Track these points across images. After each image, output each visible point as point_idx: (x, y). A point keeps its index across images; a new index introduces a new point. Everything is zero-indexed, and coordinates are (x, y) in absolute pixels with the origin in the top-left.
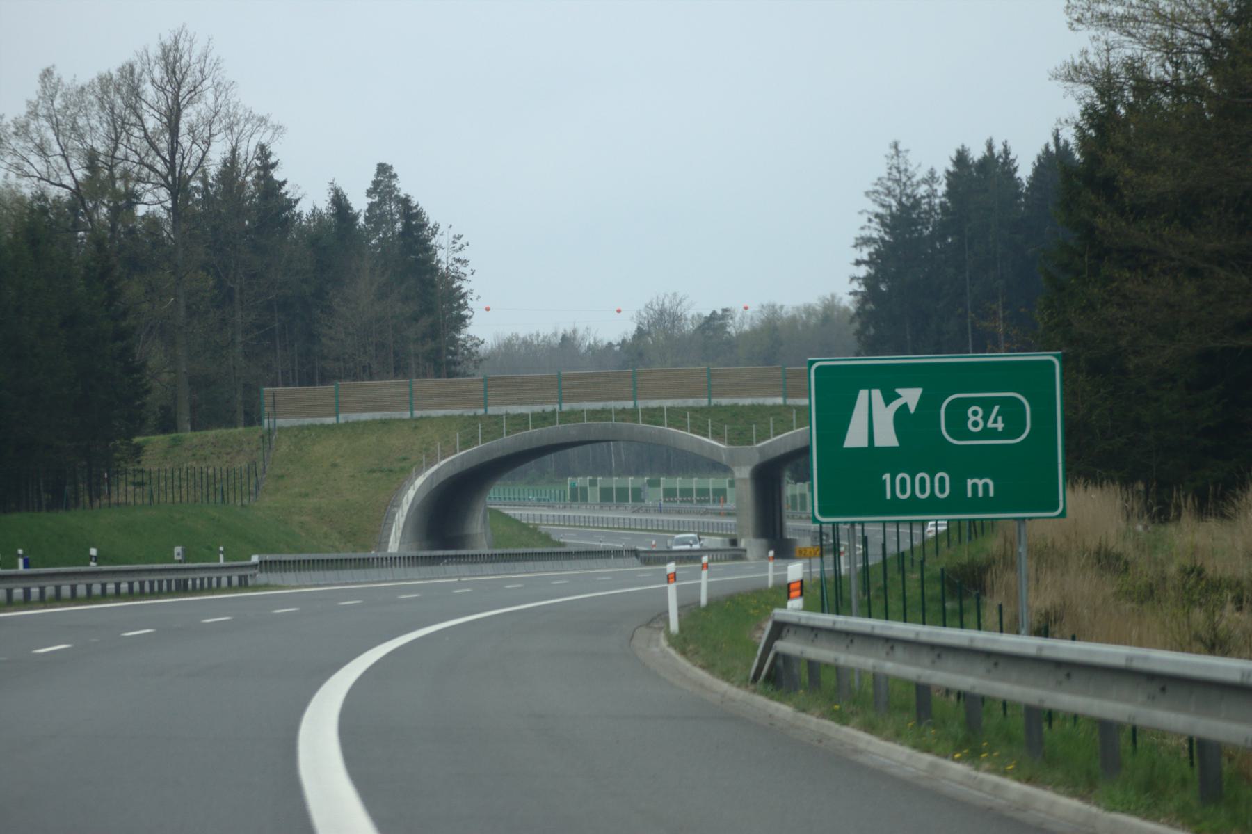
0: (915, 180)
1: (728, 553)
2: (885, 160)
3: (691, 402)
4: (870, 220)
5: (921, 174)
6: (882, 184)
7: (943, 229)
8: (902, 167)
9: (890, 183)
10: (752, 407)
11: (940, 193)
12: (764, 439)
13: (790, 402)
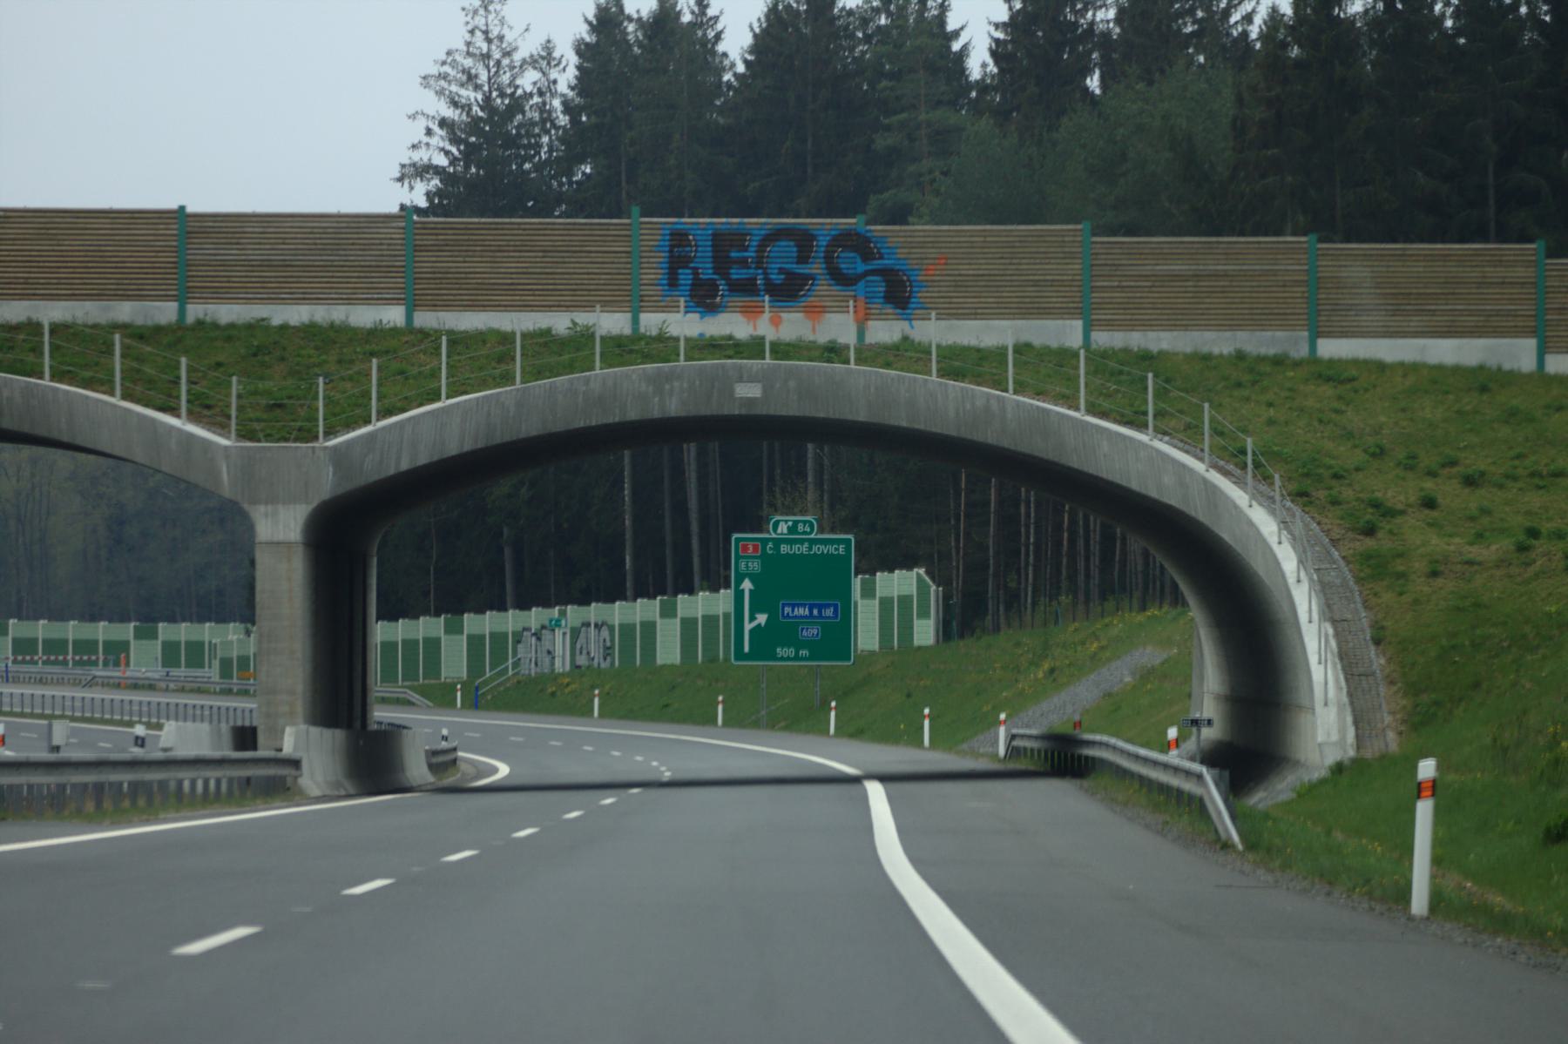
0: (517, 57)
1: (226, 773)
2: (462, 18)
3: (125, 311)
4: (429, 132)
5: (528, 47)
6: (454, 64)
7: (577, 143)
8: (494, 33)
9: (468, 62)
10: (310, 331)
11: (562, 87)
12: (350, 425)
13: (426, 319)
